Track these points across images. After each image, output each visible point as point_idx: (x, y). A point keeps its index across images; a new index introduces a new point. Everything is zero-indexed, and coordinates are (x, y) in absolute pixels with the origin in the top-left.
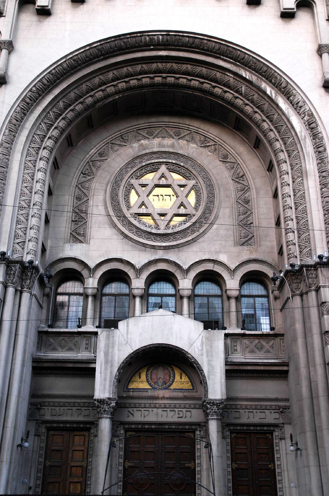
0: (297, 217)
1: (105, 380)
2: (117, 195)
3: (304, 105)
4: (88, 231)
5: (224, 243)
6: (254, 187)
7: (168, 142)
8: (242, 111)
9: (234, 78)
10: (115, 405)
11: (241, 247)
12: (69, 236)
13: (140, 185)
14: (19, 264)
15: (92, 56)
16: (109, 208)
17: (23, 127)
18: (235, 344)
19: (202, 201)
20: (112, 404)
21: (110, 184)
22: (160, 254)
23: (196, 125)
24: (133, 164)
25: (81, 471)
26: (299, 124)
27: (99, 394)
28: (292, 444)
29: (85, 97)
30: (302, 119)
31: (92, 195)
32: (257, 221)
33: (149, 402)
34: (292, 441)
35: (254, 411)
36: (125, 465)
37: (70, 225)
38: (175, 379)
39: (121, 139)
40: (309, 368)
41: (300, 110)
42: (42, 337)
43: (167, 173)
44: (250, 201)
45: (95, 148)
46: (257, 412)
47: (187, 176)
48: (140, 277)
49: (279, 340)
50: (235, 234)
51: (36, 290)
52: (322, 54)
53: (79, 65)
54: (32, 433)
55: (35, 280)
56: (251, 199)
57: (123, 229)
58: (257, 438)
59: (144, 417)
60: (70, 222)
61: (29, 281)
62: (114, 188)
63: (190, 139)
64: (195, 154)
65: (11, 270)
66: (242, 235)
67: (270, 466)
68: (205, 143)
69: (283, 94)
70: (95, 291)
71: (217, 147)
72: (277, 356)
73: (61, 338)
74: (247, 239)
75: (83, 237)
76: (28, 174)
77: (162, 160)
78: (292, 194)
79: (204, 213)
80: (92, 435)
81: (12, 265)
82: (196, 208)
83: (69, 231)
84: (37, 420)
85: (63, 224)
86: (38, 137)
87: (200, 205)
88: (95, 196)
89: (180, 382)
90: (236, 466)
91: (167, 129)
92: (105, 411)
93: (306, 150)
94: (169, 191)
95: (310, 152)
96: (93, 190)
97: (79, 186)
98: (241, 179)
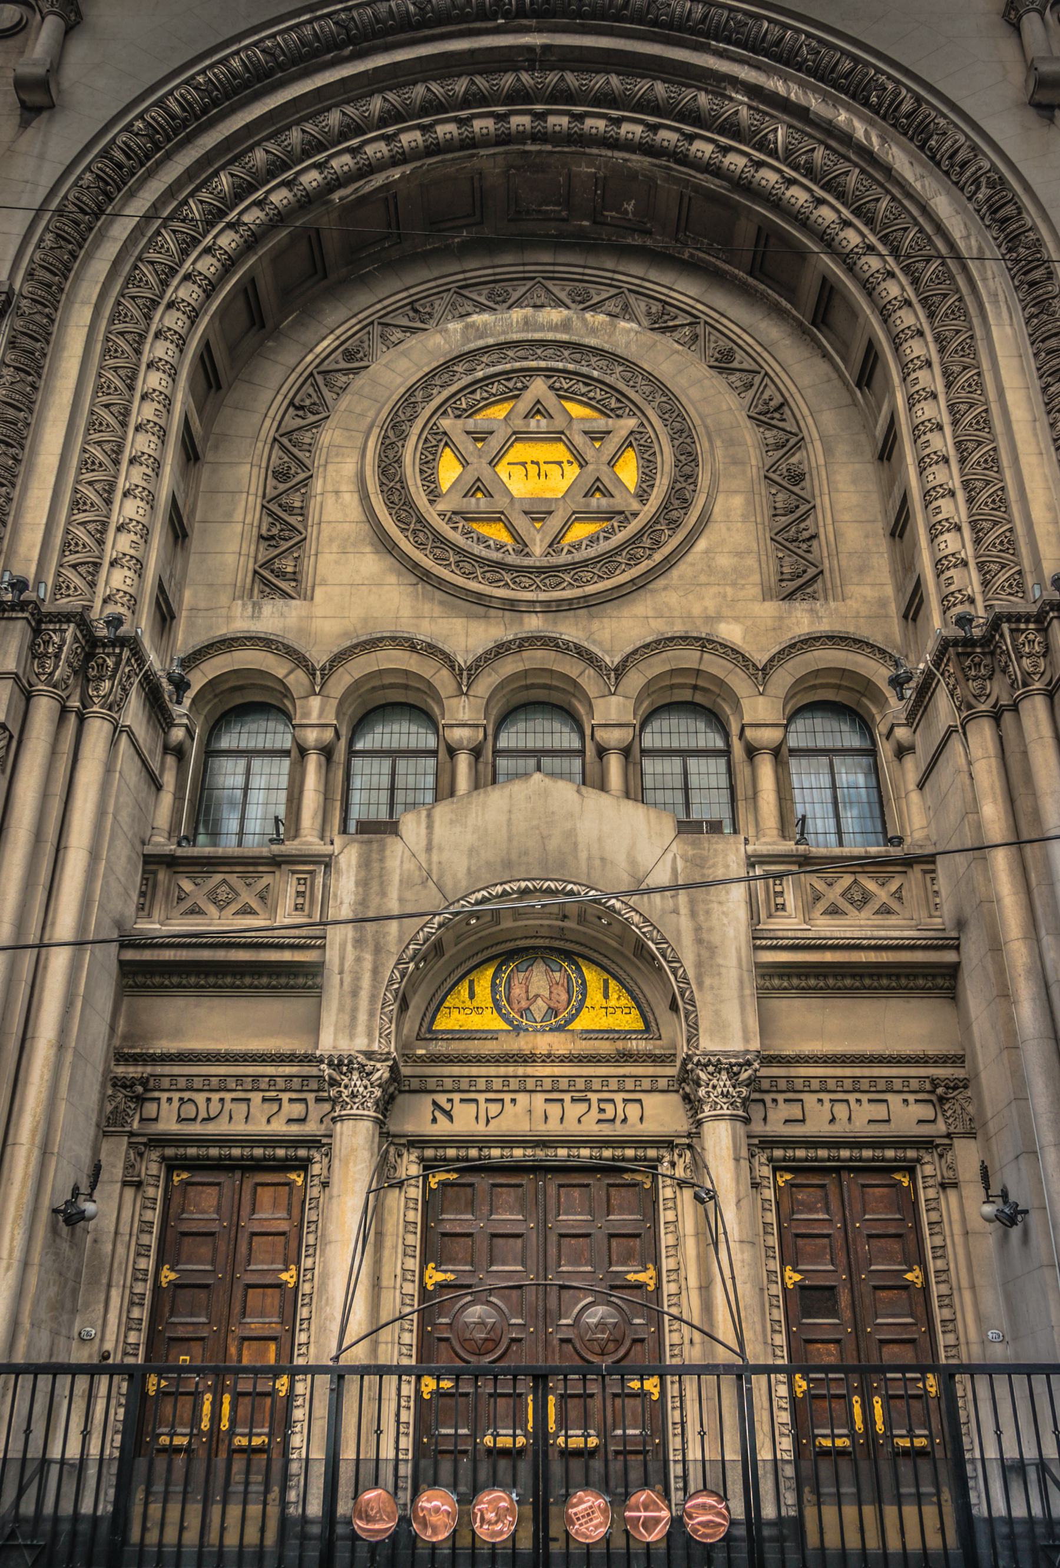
0: (966, 484)
1: (355, 993)
2: (399, 461)
3: (976, 156)
4: (308, 565)
5: (729, 590)
6: (815, 435)
7: (554, 315)
8: (777, 204)
9: (750, 107)
10: (387, 1075)
11: (785, 605)
12: (249, 580)
13: (468, 433)
14: (72, 625)
15: (319, 41)
16: (372, 497)
17: (102, 236)
18: (778, 889)
19: (659, 476)
20: (379, 1074)
21: (376, 431)
22: (534, 623)
23: (633, 272)
24: (446, 377)
25: (277, 1302)
26: (959, 217)
27: (335, 1039)
28: (988, 1196)
29: (299, 168)
30: (969, 199)
31: (322, 462)
32: (830, 528)
33: (502, 1071)
34: (987, 1188)
35: (852, 1097)
36: (427, 1279)
37: (253, 547)
38: (588, 1000)
39: (411, 314)
40: (1038, 941)
41: (961, 174)
42: (155, 873)
43: (550, 401)
44: (807, 476)
45: (332, 337)
46: (858, 1101)
47: (613, 406)
48: (471, 693)
49: (919, 875)
50: (764, 565)
51: (134, 713)
52: (1020, 18)
53: (281, 67)
54: (114, 1171)
55: (132, 684)
56: (810, 468)
57: (417, 555)
58: (863, 1186)
59: (488, 1121)
60: (255, 539)
61: (107, 684)
62: (388, 442)
63: (618, 310)
64: (634, 348)
65: (47, 643)
66: (786, 570)
67: (909, 1276)
68: (663, 321)
69: (905, 134)
70: (329, 735)
71: (700, 329)
72: (914, 923)
73: (218, 878)
74: (801, 581)
75: (293, 584)
76: (115, 369)
77: (534, 364)
78: (946, 419)
79: (665, 507)
80: (316, 1181)
81: (51, 627)
82: (642, 495)
83: (251, 566)
84: (131, 1134)
85: (230, 543)
86: (150, 268)
87: (652, 486)
88: (330, 467)
89: (606, 1009)
90: (797, 1277)
91: (549, 284)
92: (353, 1095)
93: (986, 286)
94: (559, 451)
95: (1000, 292)
96: (325, 450)
97: (285, 441)
98: (777, 415)
